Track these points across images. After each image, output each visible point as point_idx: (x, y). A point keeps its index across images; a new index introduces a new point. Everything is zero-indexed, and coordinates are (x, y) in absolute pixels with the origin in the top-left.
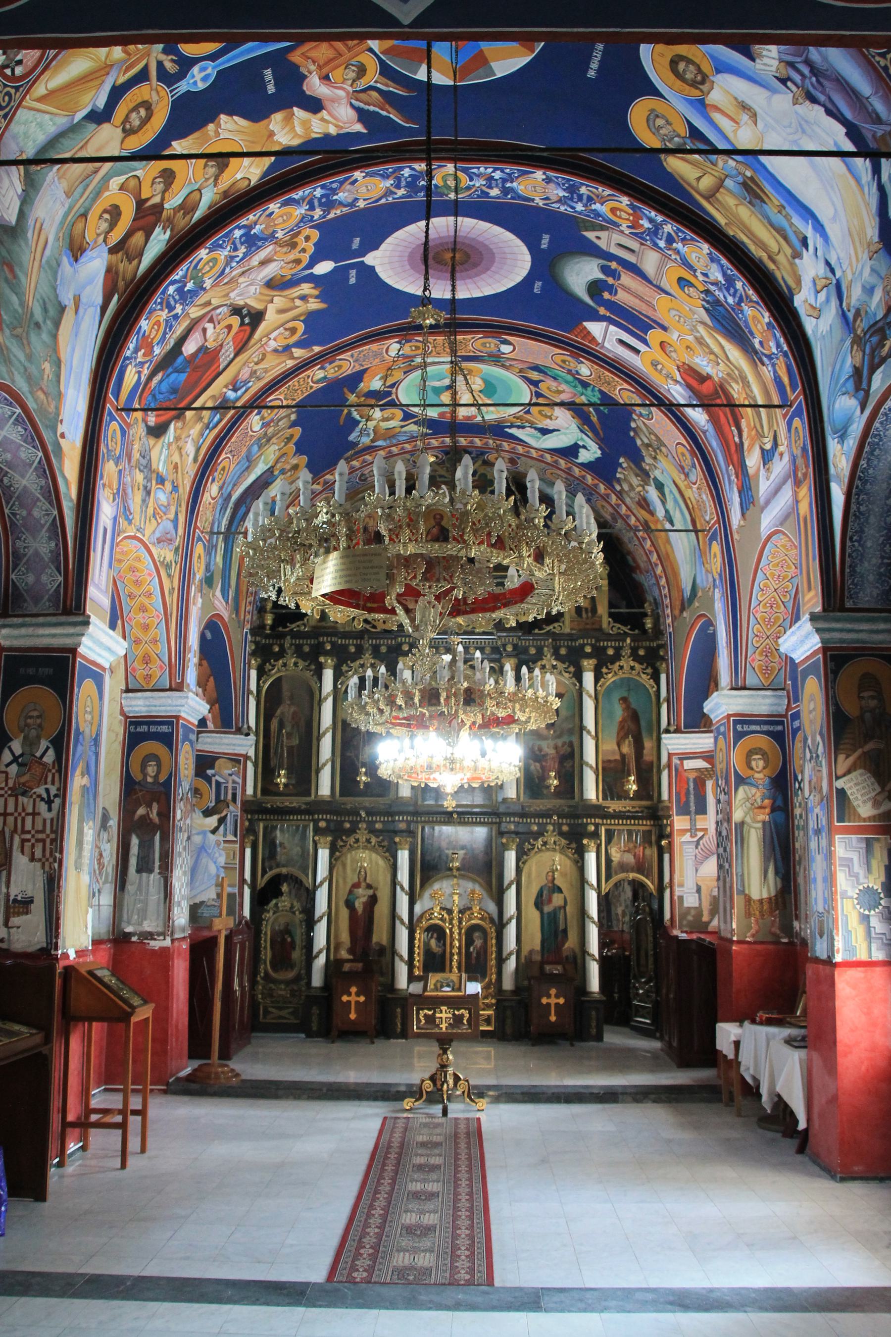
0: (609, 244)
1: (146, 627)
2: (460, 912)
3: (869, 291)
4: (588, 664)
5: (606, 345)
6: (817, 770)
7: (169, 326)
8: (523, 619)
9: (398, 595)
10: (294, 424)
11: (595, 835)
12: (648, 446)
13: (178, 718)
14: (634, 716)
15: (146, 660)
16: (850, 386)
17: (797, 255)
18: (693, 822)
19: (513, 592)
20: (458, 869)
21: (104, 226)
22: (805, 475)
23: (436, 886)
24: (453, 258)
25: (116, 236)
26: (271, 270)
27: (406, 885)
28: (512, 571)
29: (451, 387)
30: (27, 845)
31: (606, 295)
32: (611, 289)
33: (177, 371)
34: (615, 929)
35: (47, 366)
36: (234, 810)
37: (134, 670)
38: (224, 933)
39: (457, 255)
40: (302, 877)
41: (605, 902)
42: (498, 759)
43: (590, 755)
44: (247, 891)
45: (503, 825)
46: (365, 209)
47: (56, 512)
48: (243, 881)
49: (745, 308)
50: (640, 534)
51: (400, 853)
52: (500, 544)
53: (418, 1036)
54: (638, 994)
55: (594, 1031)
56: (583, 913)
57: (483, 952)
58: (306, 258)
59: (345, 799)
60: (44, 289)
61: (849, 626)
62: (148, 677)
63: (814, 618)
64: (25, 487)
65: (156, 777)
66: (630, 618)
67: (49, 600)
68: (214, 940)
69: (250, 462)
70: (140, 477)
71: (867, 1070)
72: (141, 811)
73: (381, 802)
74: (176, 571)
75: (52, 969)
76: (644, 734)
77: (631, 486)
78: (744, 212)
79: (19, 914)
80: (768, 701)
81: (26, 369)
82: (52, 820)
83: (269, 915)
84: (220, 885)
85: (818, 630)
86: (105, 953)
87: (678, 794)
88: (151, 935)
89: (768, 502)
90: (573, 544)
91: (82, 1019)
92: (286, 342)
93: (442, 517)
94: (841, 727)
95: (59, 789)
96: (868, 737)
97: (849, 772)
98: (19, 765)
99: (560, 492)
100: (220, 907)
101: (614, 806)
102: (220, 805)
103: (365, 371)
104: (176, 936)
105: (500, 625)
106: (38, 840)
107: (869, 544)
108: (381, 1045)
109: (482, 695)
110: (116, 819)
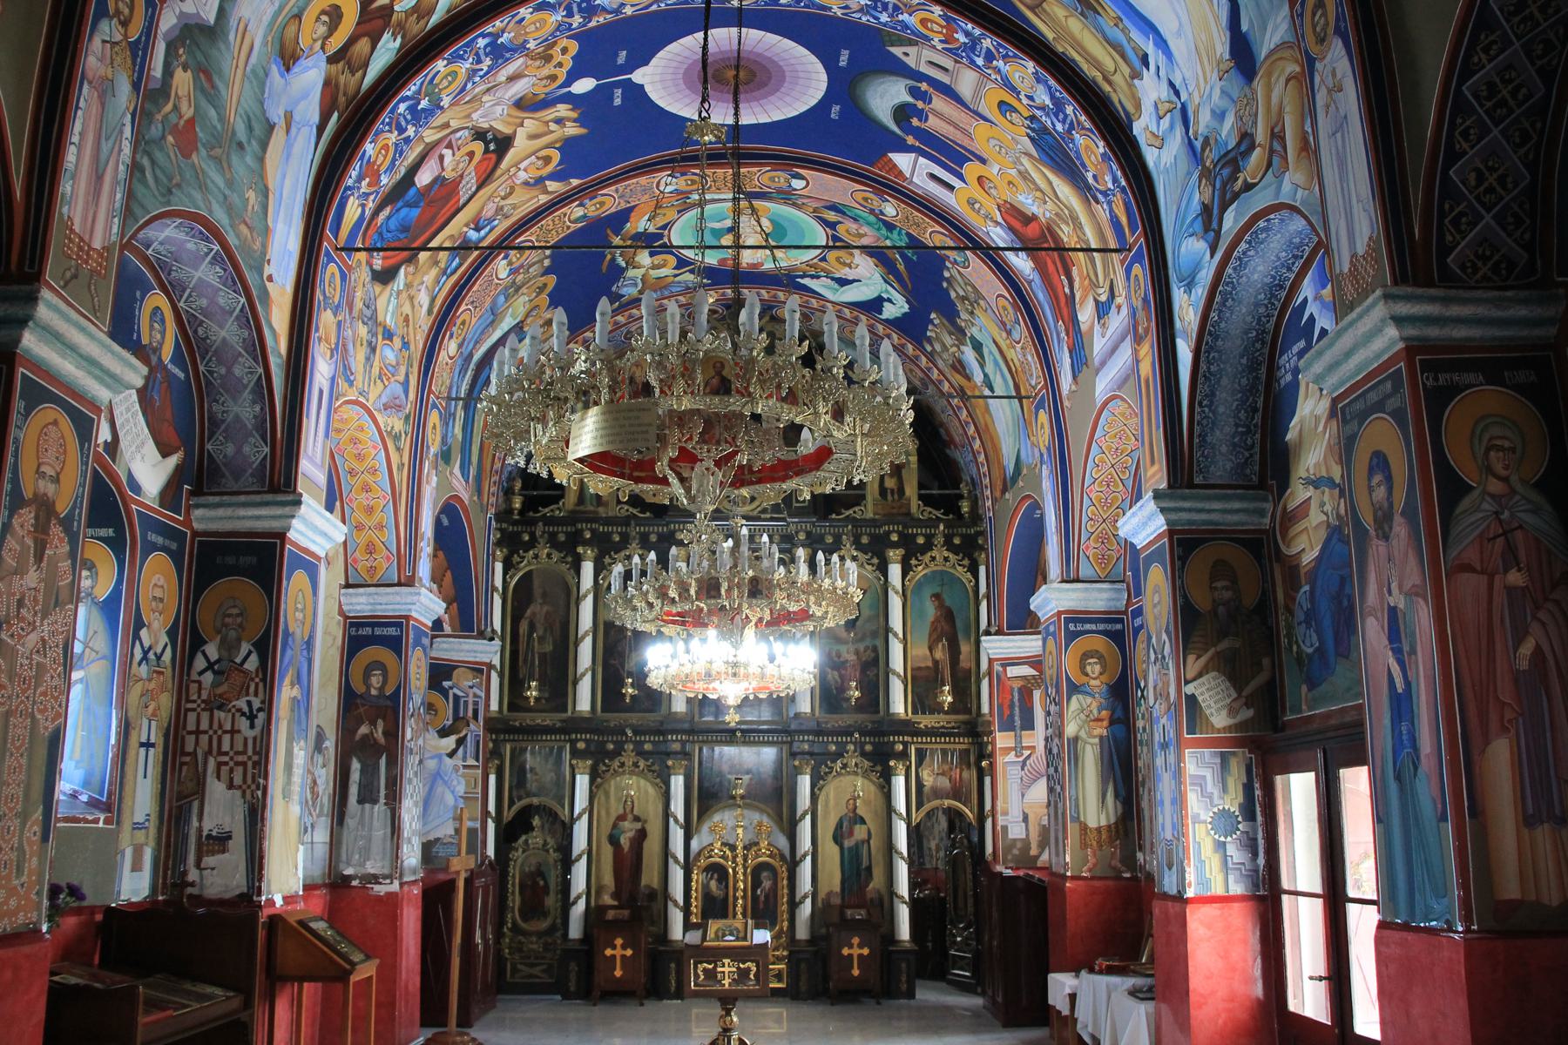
0: (918, 62)
1: (370, 510)
2: (745, 848)
3: (1220, 116)
4: (894, 554)
5: (915, 180)
6: (1161, 674)
7: (399, 152)
8: (818, 491)
9: (671, 460)
10: (547, 271)
11: (904, 755)
12: (964, 298)
13: (407, 618)
14: (948, 615)
15: (370, 549)
16: (1198, 226)
17: (1136, 75)
18: (1018, 739)
19: (806, 458)
20: (742, 797)
21: (322, 30)
22: (1147, 331)
23: (717, 818)
24: (736, 76)
25: (336, 42)
26: (520, 88)
27: (681, 817)
28: (805, 434)
29: (734, 230)
30: (225, 769)
31: (915, 122)
32: (921, 115)
33: (409, 205)
34: (928, 866)
35: (251, 195)
36: (476, 729)
37: (355, 561)
38: (463, 875)
39: (742, 74)
40: (558, 808)
41: (915, 834)
42: (793, 665)
43: (897, 661)
44: (491, 826)
45: (795, 745)
46: (632, 17)
47: (261, 370)
48: (486, 813)
49: (1077, 136)
50: (955, 401)
51: (673, 778)
52: (791, 398)
53: (696, 994)
54: (955, 942)
55: (904, 987)
56: (890, 848)
57: (773, 894)
58: (562, 74)
59: (608, 715)
60: (249, 103)
61: (1199, 505)
62: (372, 570)
63: (1158, 496)
64: (224, 339)
65: (381, 689)
66: (939, 501)
67: (252, 475)
68: (451, 884)
69: (495, 316)
70: (363, 331)
71: (1225, 1023)
72: (364, 730)
73: (651, 718)
74: (406, 443)
75: (255, 917)
76: (960, 637)
77: (944, 345)
78: (1075, 25)
79: (213, 853)
80: (1105, 595)
81: (225, 197)
82: (255, 739)
83: (517, 855)
84: (459, 818)
85: (1162, 510)
86: (318, 904)
87: (1000, 706)
88: (375, 879)
89: (1103, 363)
90: (879, 399)
91: (292, 979)
92: (540, 173)
93: (723, 366)
94: (1192, 624)
95: (263, 702)
96: (1223, 634)
97: (1200, 675)
98: (215, 673)
99: (863, 337)
100: (459, 845)
101: (926, 721)
102: (460, 724)
103: (630, 210)
104: (406, 879)
105: (789, 498)
106: (237, 764)
107: (1221, 409)
108: (651, 1006)
109: (771, 586)
110: (333, 739)
